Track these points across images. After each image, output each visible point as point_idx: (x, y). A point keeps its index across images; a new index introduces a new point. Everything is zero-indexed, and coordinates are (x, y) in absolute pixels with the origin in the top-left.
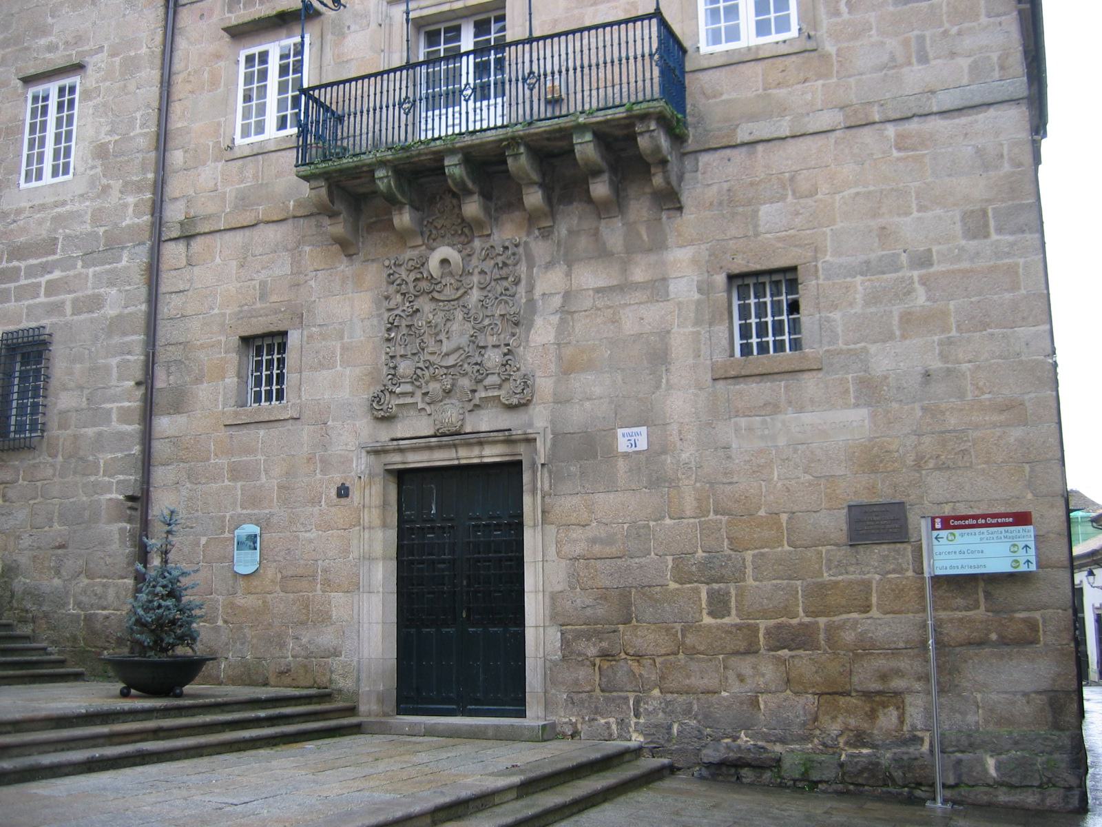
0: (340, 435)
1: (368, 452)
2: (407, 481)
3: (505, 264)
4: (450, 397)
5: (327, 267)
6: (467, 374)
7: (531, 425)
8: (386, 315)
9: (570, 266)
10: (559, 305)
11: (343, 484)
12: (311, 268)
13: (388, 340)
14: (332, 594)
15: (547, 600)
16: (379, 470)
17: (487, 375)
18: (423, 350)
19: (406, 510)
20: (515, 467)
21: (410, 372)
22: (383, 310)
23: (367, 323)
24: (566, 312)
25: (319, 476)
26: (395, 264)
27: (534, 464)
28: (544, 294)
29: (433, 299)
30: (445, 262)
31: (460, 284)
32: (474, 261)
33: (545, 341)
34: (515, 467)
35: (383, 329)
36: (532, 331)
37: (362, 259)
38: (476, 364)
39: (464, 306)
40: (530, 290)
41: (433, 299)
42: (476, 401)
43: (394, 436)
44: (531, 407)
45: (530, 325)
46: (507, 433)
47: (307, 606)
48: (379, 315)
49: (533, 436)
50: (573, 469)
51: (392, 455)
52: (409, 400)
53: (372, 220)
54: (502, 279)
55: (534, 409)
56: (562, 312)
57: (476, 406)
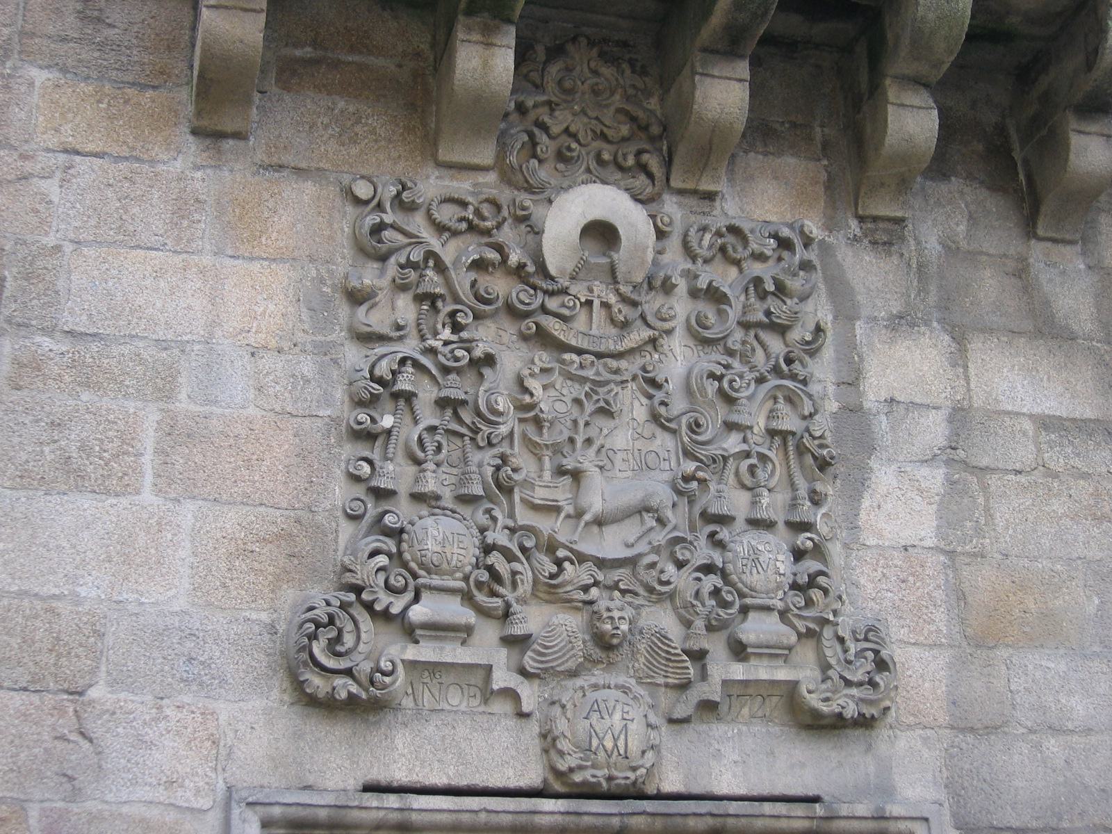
0: (141, 742)
3: (781, 290)
5: (115, 150)
7: (887, 790)
9: (960, 338)
10: (942, 442)
13: (366, 436)
17: (745, 610)
18: (508, 491)
21: (464, 552)
22: (339, 334)
23: (268, 362)
28: (891, 401)
29: (543, 338)
30: (601, 233)
33: (908, 536)
36: (866, 503)
37: (260, 156)
38: (708, 569)
40: (851, 380)
44: (882, 733)
45: (858, 486)
48: (324, 349)
53: (298, 53)
56: (949, 462)
57: (708, 707)
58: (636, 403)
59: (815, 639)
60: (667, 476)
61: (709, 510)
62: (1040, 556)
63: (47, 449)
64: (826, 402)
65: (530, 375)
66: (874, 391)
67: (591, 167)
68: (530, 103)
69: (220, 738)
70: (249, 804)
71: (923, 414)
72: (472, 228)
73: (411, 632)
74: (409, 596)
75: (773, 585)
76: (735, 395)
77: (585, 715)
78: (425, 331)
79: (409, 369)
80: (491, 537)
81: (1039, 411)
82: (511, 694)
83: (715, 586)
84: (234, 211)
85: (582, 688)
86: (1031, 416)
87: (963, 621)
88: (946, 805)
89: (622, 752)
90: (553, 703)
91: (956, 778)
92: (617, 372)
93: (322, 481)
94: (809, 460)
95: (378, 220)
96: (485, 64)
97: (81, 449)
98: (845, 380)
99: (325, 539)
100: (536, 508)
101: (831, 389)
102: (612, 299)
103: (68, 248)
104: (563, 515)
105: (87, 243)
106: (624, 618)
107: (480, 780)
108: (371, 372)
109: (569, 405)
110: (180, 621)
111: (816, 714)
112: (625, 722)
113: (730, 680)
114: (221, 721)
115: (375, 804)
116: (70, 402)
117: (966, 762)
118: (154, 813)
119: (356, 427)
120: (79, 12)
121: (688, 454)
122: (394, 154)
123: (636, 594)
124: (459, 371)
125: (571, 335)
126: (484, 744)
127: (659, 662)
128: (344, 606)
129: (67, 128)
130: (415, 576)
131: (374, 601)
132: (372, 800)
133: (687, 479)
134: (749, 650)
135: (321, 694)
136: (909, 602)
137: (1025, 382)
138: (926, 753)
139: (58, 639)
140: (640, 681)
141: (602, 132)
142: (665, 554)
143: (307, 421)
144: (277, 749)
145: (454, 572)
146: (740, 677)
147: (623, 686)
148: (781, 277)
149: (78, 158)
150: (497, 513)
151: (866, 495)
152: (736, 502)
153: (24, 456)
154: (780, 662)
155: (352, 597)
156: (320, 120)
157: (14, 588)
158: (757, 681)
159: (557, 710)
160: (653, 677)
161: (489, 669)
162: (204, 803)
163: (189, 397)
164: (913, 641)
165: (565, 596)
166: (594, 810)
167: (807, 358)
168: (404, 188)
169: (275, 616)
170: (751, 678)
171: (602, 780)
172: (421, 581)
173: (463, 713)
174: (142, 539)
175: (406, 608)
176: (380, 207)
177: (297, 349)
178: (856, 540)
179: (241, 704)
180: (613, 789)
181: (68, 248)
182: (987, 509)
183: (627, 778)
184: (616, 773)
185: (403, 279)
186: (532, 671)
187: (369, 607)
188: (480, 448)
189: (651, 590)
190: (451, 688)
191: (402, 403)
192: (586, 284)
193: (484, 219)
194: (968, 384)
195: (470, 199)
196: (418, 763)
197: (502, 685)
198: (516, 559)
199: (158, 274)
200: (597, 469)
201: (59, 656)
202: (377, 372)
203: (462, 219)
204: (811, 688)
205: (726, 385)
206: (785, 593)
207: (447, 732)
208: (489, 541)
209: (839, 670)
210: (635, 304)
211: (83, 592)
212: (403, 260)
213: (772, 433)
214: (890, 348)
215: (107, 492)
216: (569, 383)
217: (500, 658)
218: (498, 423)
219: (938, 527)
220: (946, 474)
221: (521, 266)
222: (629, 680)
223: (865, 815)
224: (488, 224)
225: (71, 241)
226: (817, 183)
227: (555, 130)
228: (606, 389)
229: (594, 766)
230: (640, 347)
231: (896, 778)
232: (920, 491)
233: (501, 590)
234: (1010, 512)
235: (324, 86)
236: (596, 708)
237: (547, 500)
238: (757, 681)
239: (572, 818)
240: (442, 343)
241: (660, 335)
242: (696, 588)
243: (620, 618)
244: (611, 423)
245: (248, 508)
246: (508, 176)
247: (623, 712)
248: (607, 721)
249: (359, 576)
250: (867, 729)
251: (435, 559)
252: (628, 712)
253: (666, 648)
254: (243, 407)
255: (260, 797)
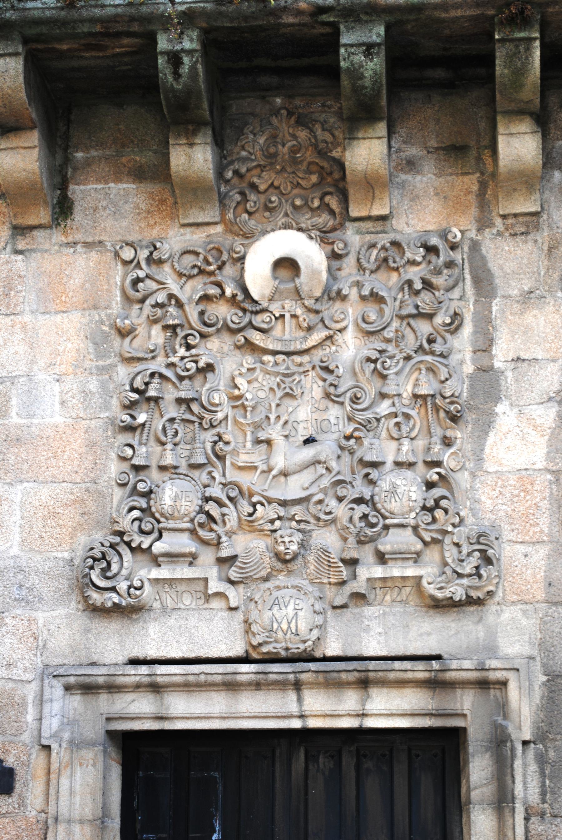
3: (428, 285)
7: (492, 650)
17: (386, 527)
18: (221, 458)
21: (190, 505)
27: (500, 744)
29: (250, 347)
30: (286, 265)
38: (360, 501)
40: (484, 346)
44: (492, 607)
45: (486, 425)
57: (359, 597)
58: (315, 386)
59: (440, 545)
61: (364, 458)
64: (464, 367)
65: (240, 374)
66: (501, 355)
67: (289, 212)
68: (243, 170)
69: (38, 636)
70: (54, 676)
71: (542, 366)
72: (202, 272)
74: (155, 535)
75: (406, 509)
76: (385, 372)
77: (269, 608)
78: (169, 351)
79: (156, 380)
80: (209, 492)
82: (220, 595)
83: (364, 513)
84: (43, 281)
85: (269, 589)
89: (294, 631)
90: (251, 600)
91: (548, 639)
93: (103, 462)
94: (442, 414)
95: (135, 275)
96: (190, 158)
98: (480, 348)
99: (105, 501)
100: (240, 468)
101: (468, 356)
104: (259, 472)
106: (292, 542)
108: (131, 385)
109: (268, 392)
110: (15, 562)
111: (433, 598)
112: (296, 611)
113: (372, 578)
114: (39, 625)
115: (133, 672)
117: (557, 627)
119: (122, 424)
122: (152, 222)
123: (308, 522)
124: (190, 378)
125: (269, 342)
126: (207, 629)
127: (324, 568)
128: (112, 546)
130: (159, 522)
131: (131, 541)
132: (131, 670)
133: (348, 438)
134: (387, 556)
135: (99, 604)
136: (519, 511)
138: (524, 622)
140: (312, 582)
141: (298, 183)
142: (331, 492)
143: (93, 422)
144: (74, 640)
145: (184, 517)
147: (297, 586)
148: (428, 277)
150: (216, 474)
151: (491, 434)
152: (389, 452)
154: (411, 563)
155: (118, 539)
156: (100, 204)
158: (392, 578)
159: (252, 605)
160: (320, 578)
161: (206, 580)
162: (29, 676)
163: (17, 414)
164: (520, 540)
165: (259, 527)
166: (275, 670)
167: (448, 336)
168: (155, 248)
169: (73, 554)
170: (387, 576)
171: (280, 650)
172: (161, 525)
173: (193, 609)
175: (151, 546)
177: (87, 372)
178: (481, 469)
179: (52, 612)
180: (289, 655)
183: (298, 648)
184: (290, 645)
185: (153, 316)
186: (236, 580)
187: (128, 544)
188: (206, 429)
189: (318, 519)
190: (184, 594)
191: (152, 404)
192: (280, 303)
193: (209, 264)
195: (200, 250)
196: (163, 644)
197: (215, 590)
200: (283, 438)
202: (135, 386)
203: (194, 266)
205: (379, 366)
206: (417, 514)
207: (182, 622)
208: (207, 494)
209: (453, 566)
210: (317, 312)
212: (153, 303)
213: (416, 396)
214: (519, 318)
216: (268, 376)
217: (213, 573)
218: (216, 412)
219: (548, 453)
220: (558, 412)
221: (234, 296)
222: (303, 582)
223: (470, 667)
224: (212, 268)
226: (469, 193)
227: (262, 187)
228: (291, 379)
229: (276, 641)
230: (319, 344)
231: (500, 640)
232: (535, 427)
233: (215, 527)
235: (103, 177)
236: (276, 602)
237: (247, 463)
239: (261, 676)
240: (179, 358)
241: (335, 333)
242: (350, 515)
243: (290, 542)
244: (295, 403)
245: (55, 485)
246: (231, 228)
247: (295, 604)
248: (284, 612)
249: (121, 525)
250: (479, 605)
251: (169, 510)
252: (298, 604)
253: (327, 558)
255: (61, 671)
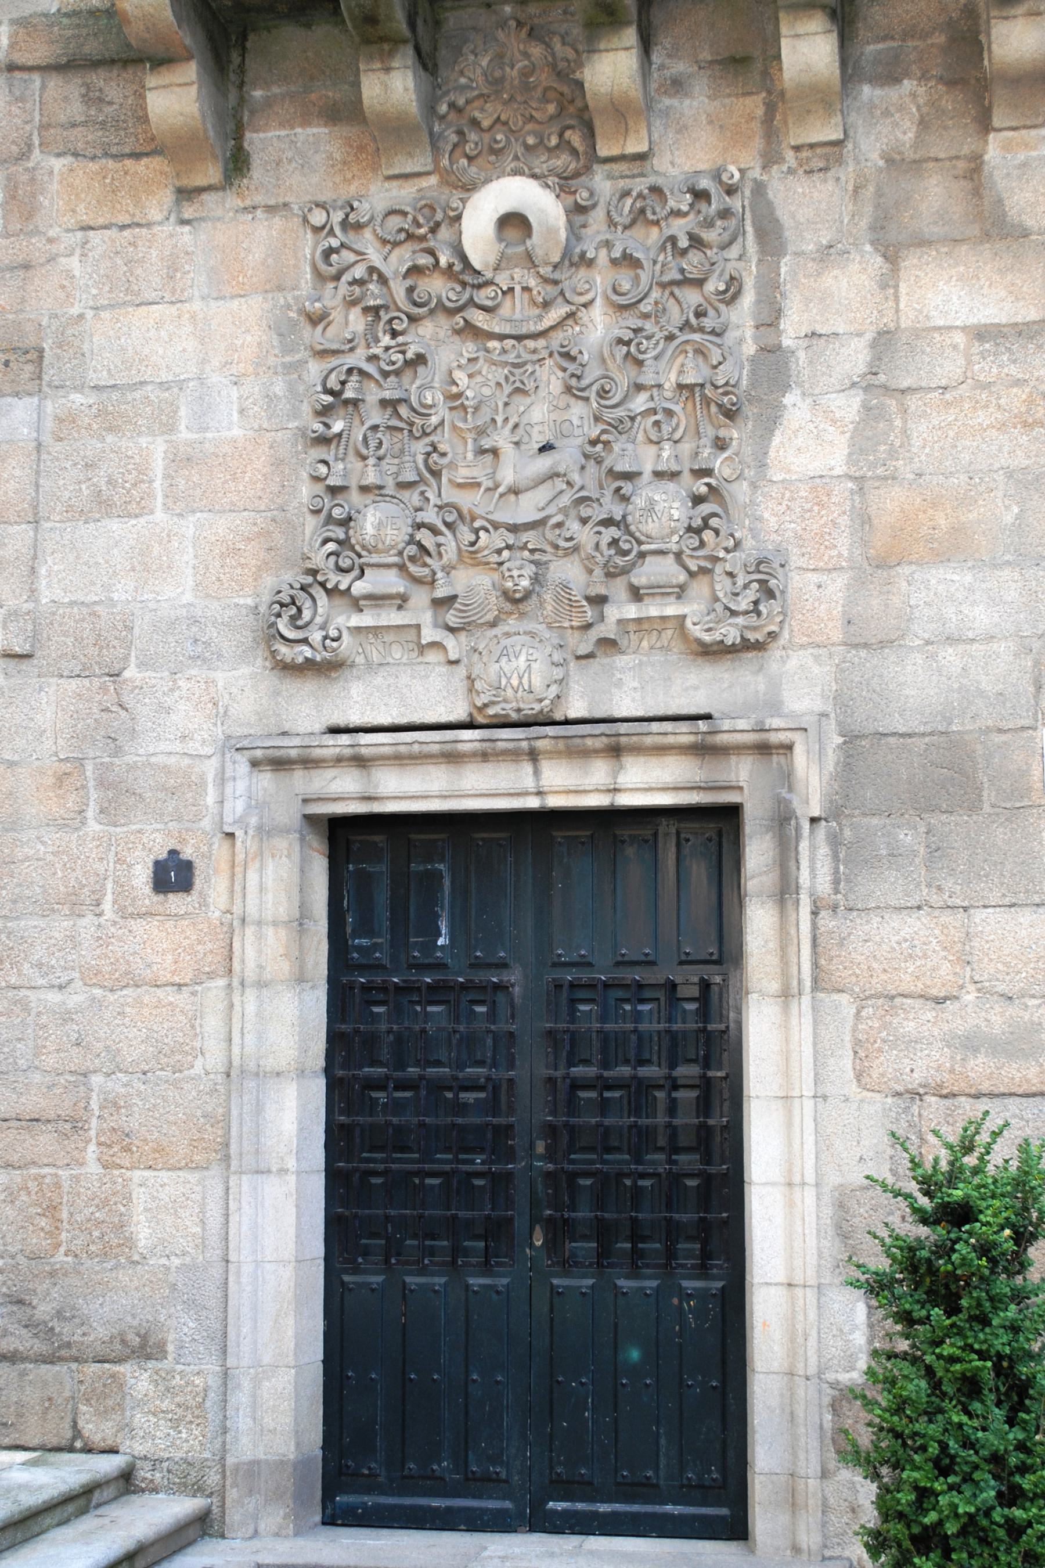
1: (255, 764)
2: (375, 862)
3: (696, 242)
4: (522, 615)
6: (576, 549)
7: (775, 706)
8: (315, 370)
9: (892, 255)
10: (862, 368)
11: (173, 853)
12: (71, 221)
13: (323, 441)
14: (137, 1175)
15: (828, 1211)
16: (289, 814)
17: (642, 555)
18: (436, 474)
19: (356, 934)
20: (715, 826)
21: (396, 534)
24: (882, 388)
25: (93, 826)
26: (345, 224)
27: (783, 820)
29: (470, 330)
30: (514, 223)
31: (551, 290)
32: (597, 219)
33: (815, 467)
34: (715, 826)
35: (306, 409)
36: (777, 439)
38: (608, 522)
39: (567, 356)
40: (770, 319)
41: (470, 330)
42: (608, 629)
43: (340, 721)
44: (775, 652)
45: (771, 419)
46: (702, 726)
47: (52, 1209)
49: (782, 737)
50: (906, 837)
51: (330, 773)
52: (392, 617)
54: (686, 282)
55: (783, 661)
56: (867, 389)
57: (608, 644)
58: (553, 378)
60: (579, 441)
62: (958, 471)
63: (84, 487)
68: (461, 102)
72: (410, 237)
73: (357, 604)
74: (356, 572)
76: (641, 357)
79: (355, 378)
81: (975, 321)
86: (964, 329)
87: (865, 543)
88: (833, 715)
92: (534, 351)
94: (714, 409)
97: (109, 482)
100: (460, 486)
102: (532, 283)
103: (90, 314)
104: (482, 489)
105: (103, 308)
107: (417, 718)
108: (324, 385)
115: (331, 743)
116: (100, 445)
118: (172, 760)
120: (83, 96)
121: (597, 419)
123: (544, 552)
128: (303, 588)
129: (81, 208)
130: (360, 556)
132: (330, 740)
133: (593, 443)
137: (962, 293)
138: (816, 670)
139: (99, 635)
140: (550, 627)
146: (633, 616)
148: (696, 231)
149: (91, 233)
150: (429, 494)
151: (777, 433)
152: (647, 460)
153: (67, 494)
155: (310, 579)
157: (67, 600)
161: (418, 627)
162: (208, 750)
165: (484, 560)
166: (505, 737)
174: (156, 550)
176: (331, 233)
181: (90, 314)
182: (904, 431)
184: (522, 706)
187: (323, 585)
190: (394, 646)
191: (351, 408)
194: (897, 304)
195: (408, 209)
197: (430, 640)
198: (441, 533)
199: (159, 325)
201: (101, 648)
202: (328, 386)
203: (401, 230)
204: (695, 620)
205: (633, 349)
211: (116, 596)
213: (681, 387)
215: (130, 516)
216: (494, 368)
217: (427, 618)
219: (850, 454)
221: (450, 266)
225: (91, 308)
227: (486, 123)
228: (522, 370)
229: (505, 701)
232: (834, 422)
233: (428, 560)
234: (924, 430)
236: (504, 653)
238: (648, 618)
239: (488, 744)
248: (514, 664)
254: (229, 429)
255: (245, 743)
